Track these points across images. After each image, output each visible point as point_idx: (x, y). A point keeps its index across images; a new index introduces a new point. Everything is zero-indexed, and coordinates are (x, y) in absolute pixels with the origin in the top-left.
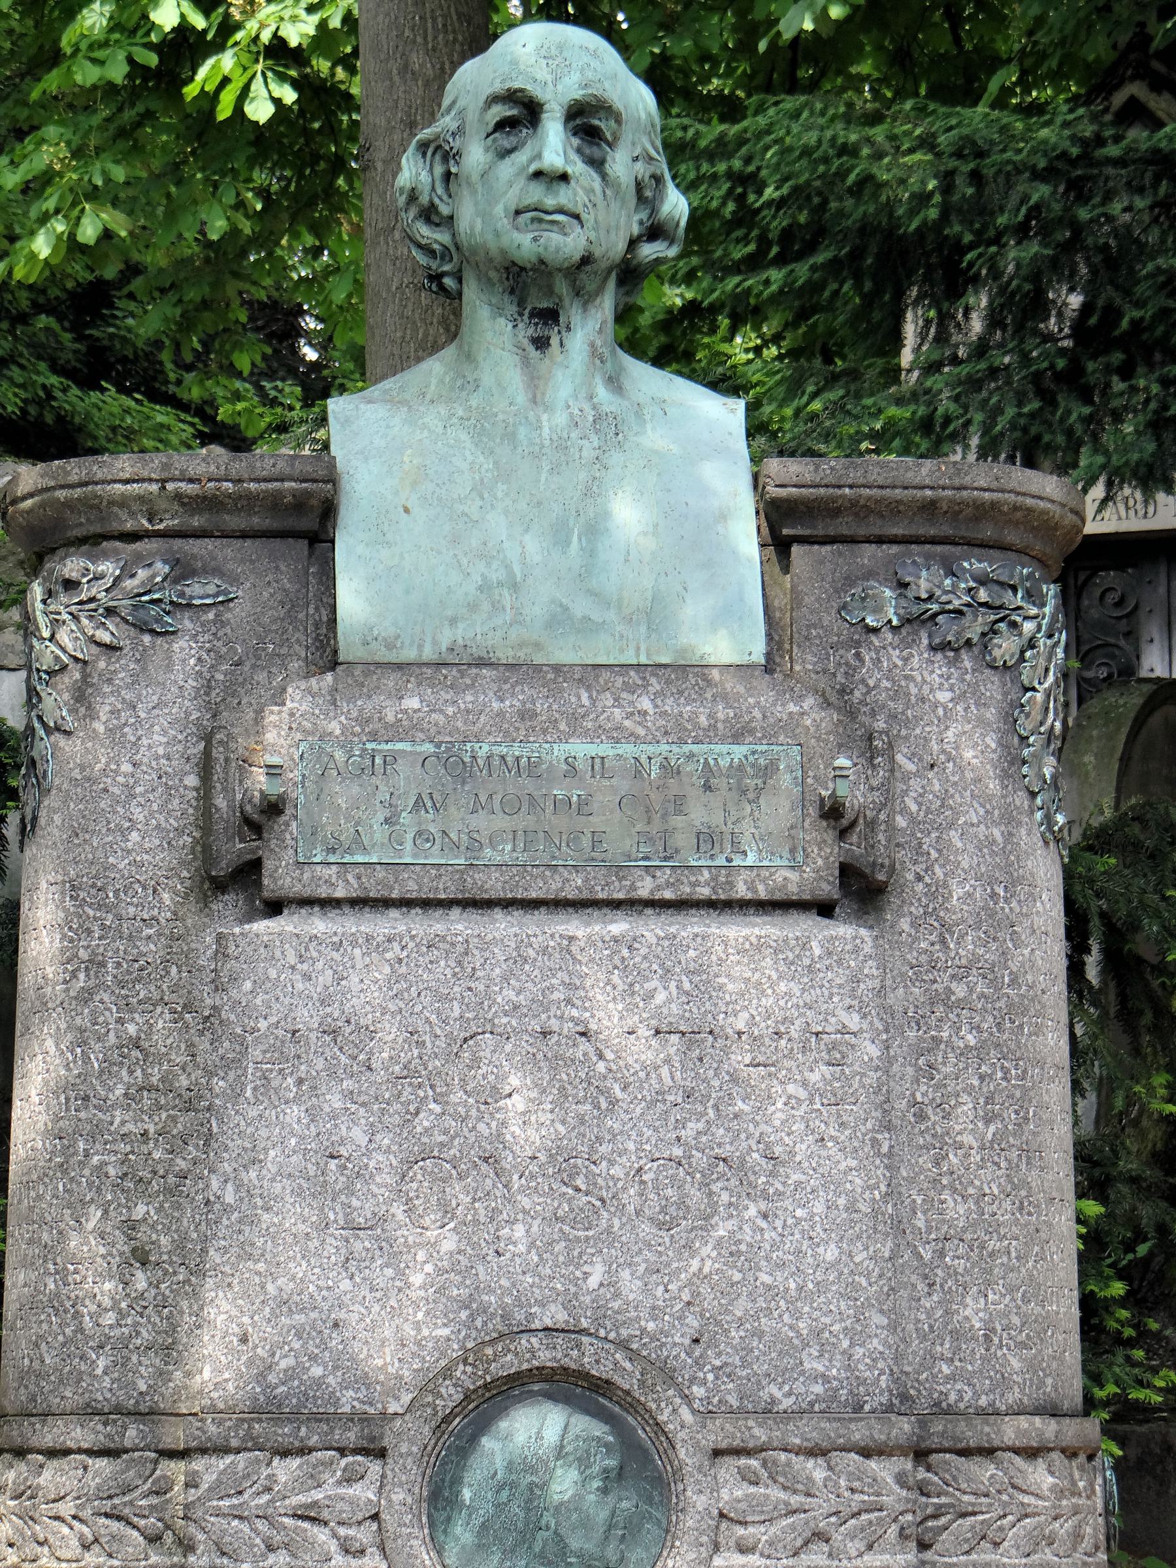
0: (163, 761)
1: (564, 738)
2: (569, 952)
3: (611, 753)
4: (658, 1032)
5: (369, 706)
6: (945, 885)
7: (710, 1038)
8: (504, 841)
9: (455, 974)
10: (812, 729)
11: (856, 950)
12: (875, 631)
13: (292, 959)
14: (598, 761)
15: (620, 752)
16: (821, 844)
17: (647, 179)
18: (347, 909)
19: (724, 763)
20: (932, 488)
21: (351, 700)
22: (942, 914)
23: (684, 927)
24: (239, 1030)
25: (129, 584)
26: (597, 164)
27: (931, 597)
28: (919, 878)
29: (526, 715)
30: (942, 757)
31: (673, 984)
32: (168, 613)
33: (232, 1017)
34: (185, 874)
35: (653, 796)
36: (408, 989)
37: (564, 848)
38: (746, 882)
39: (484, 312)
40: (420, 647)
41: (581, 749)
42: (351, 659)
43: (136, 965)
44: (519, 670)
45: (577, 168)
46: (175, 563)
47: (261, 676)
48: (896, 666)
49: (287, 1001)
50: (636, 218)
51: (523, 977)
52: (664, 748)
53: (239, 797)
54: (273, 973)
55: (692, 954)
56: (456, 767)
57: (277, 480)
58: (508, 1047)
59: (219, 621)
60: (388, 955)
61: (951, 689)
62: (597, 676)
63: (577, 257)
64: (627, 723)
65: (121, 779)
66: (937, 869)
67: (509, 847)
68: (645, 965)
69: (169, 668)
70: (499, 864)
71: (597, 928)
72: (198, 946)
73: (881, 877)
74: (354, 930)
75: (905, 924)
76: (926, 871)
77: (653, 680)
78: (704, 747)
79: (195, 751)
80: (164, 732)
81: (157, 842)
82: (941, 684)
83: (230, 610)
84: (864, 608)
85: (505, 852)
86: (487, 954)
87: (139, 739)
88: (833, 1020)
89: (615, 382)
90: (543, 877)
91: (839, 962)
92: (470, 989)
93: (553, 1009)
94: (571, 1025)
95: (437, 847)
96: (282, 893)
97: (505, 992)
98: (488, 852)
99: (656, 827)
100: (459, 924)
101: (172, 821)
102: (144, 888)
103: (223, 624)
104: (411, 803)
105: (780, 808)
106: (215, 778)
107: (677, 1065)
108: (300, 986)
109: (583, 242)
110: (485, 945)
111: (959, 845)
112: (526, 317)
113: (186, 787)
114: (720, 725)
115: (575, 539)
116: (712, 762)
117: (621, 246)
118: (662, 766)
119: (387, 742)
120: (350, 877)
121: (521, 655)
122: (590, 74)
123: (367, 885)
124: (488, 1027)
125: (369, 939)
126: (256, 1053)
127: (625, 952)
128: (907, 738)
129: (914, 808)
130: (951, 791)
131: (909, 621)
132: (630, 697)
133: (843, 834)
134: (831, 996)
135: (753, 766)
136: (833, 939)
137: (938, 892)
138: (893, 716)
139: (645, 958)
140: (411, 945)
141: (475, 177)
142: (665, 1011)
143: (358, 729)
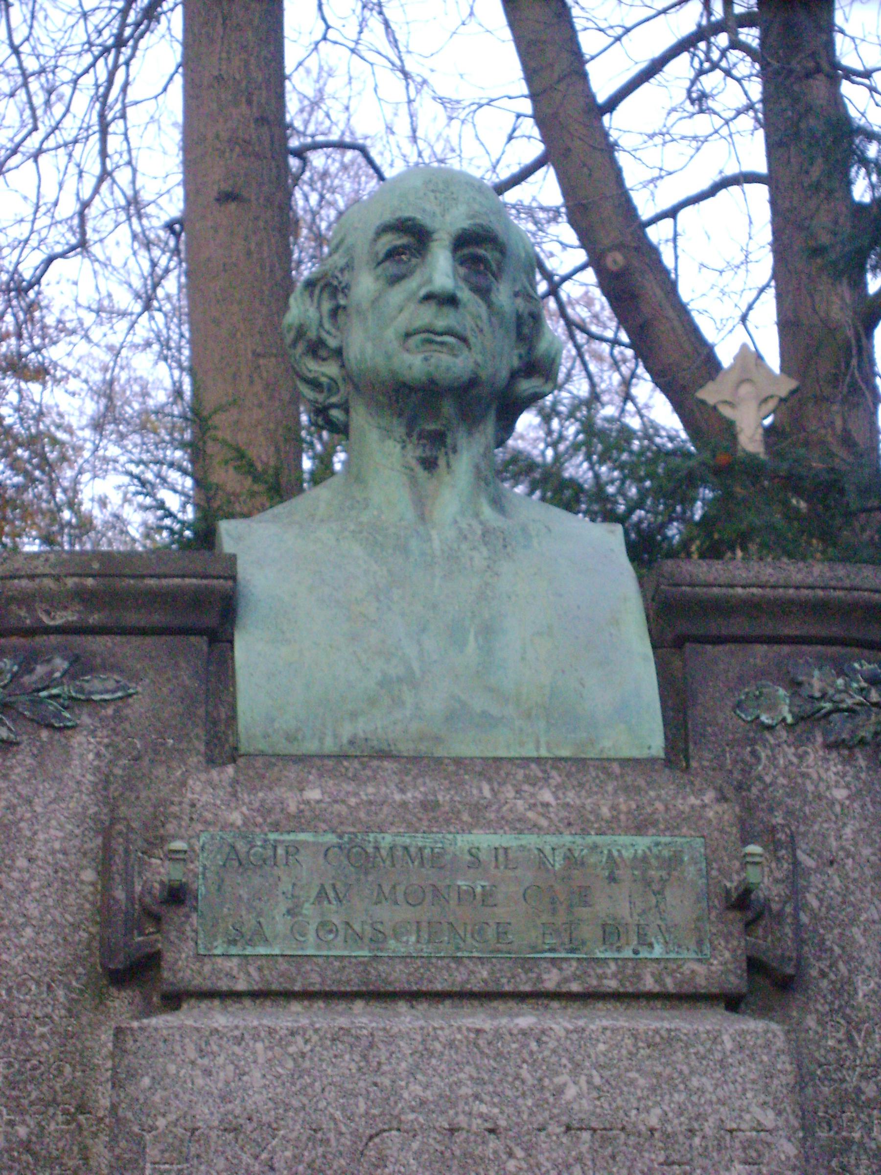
0: (60, 856)
1: (467, 829)
2: (476, 1045)
3: (514, 843)
4: (568, 1128)
5: (271, 797)
6: (850, 982)
7: (623, 1136)
8: (408, 933)
9: (359, 1069)
10: (714, 822)
11: (768, 1045)
12: (770, 728)
13: (192, 1054)
14: (501, 851)
15: (524, 842)
16: (727, 937)
17: (526, 316)
18: (247, 1002)
19: (627, 854)
20: (823, 588)
21: (253, 790)
22: (848, 1011)
23: (592, 1020)
24: (136, 1129)
25: (26, 679)
26: (483, 293)
27: (824, 696)
28: (823, 975)
29: (429, 806)
30: (842, 854)
31: (583, 1080)
32: (66, 708)
33: (129, 1115)
34: (80, 970)
35: (557, 887)
36: (312, 1085)
37: (469, 940)
38: (653, 974)
39: (373, 435)
40: (321, 740)
41: (484, 840)
42: (251, 750)
43: (28, 1066)
44: (421, 763)
45: (465, 295)
46: (75, 660)
47: (161, 771)
48: (792, 763)
49: (187, 1097)
50: (516, 352)
51: (430, 1072)
52: (567, 839)
53: (138, 888)
54: (172, 1069)
55: (601, 1047)
56: (360, 859)
57: (178, 576)
58: (415, 1145)
59: (118, 717)
60: (292, 1049)
61: (847, 786)
62: (498, 769)
63: (465, 378)
64: (530, 815)
65: (16, 875)
66: (841, 966)
67: (413, 939)
68: (554, 1059)
69: (67, 763)
70: (403, 953)
71: (504, 1021)
72: (93, 1044)
73: (790, 970)
74: (256, 1023)
75: (811, 1021)
76: (830, 967)
77: (554, 773)
78: (607, 839)
79: (93, 845)
80: (61, 828)
81: (52, 937)
82: (837, 782)
83: (128, 705)
84: (758, 707)
85: (409, 944)
86: (393, 1048)
87: (35, 833)
88: (747, 1117)
89: (498, 503)
90: (448, 968)
91: (752, 1057)
92: (376, 1084)
93: (461, 1104)
94: (479, 1121)
95: (340, 938)
96: (181, 986)
97: (412, 1087)
98: (392, 943)
99: (561, 918)
100: (362, 1017)
101: (68, 916)
102: (38, 984)
103: (123, 719)
104: (314, 893)
105: (681, 905)
106: (114, 868)
107: (589, 1163)
108: (200, 1082)
109: (471, 365)
110: (391, 1038)
111: (862, 941)
112: (414, 439)
113: (82, 882)
114: (622, 817)
115: (471, 638)
116: (615, 854)
117: (504, 374)
118: (566, 858)
119: (289, 832)
120: (252, 970)
121: (423, 748)
122: (477, 207)
123: (269, 977)
124: (395, 1124)
125: (271, 1032)
126: (153, 1152)
127: (534, 1046)
128: (804, 835)
129: (815, 903)
130: (852, 887)
131: (802, 718)
132: (531, 789)
133: (749, 926)
134: (744, 1091)
135: (657, 857)
136: (743, 1033)
137: (843, 989)
138: (789, 813)
139: (554, 1051)
140: (315, 1038)
141: (365, 305)
142: (576, 1107)
143: (260, 820)
